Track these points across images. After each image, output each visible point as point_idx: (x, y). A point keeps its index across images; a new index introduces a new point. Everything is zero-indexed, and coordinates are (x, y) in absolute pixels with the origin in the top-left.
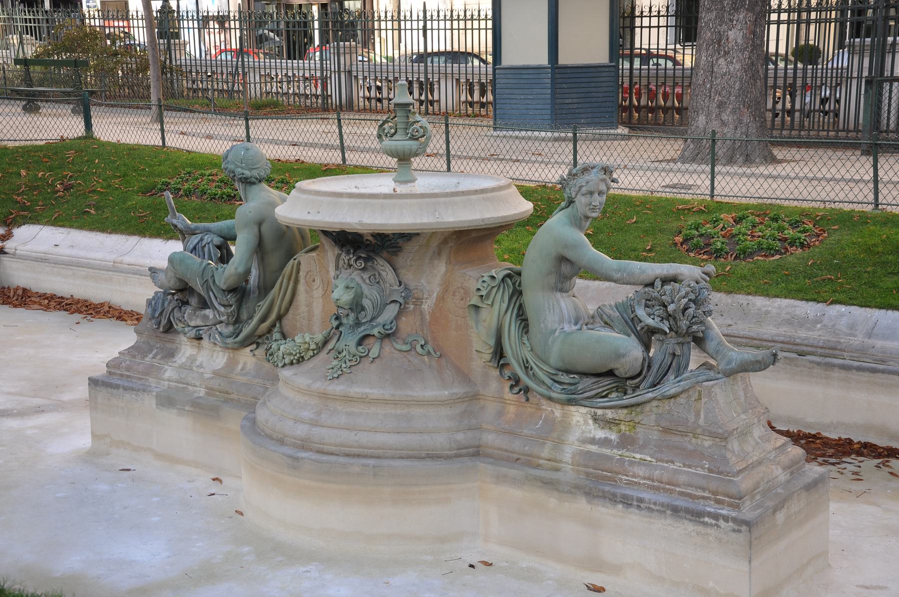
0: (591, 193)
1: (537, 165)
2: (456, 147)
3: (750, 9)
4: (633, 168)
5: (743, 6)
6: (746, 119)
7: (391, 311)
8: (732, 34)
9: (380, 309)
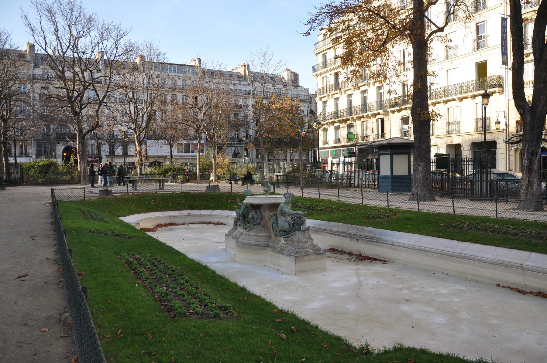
0: (287, 198)
1: (407, 204)
2: (451, 204)
3: (424, 162)
4: (400, 202)
5: (422, 161)
6: (424, 190)
7: (259, 220)
8: (420, 168)
9: (257, 219)
